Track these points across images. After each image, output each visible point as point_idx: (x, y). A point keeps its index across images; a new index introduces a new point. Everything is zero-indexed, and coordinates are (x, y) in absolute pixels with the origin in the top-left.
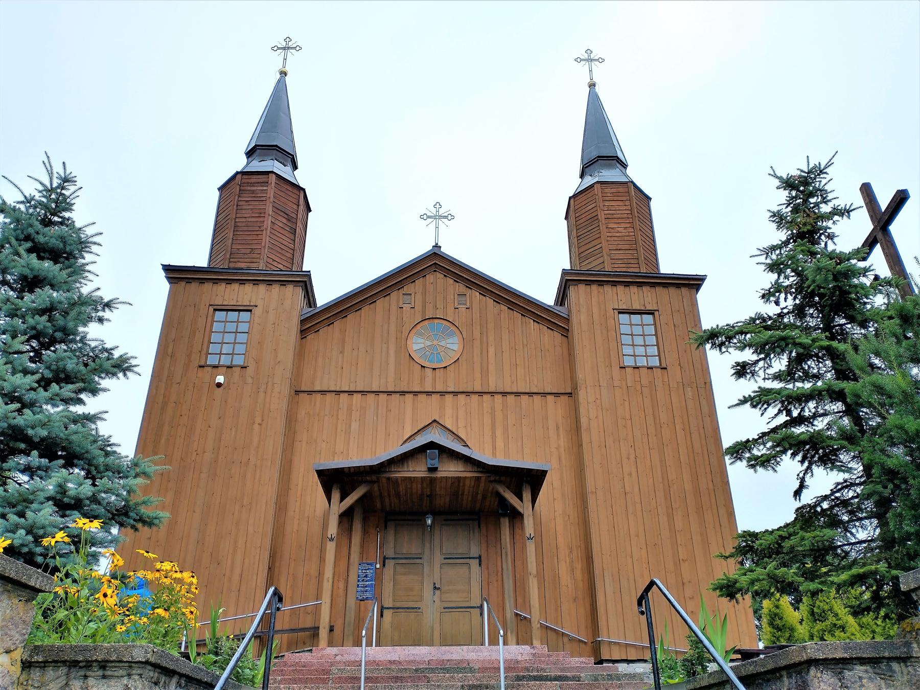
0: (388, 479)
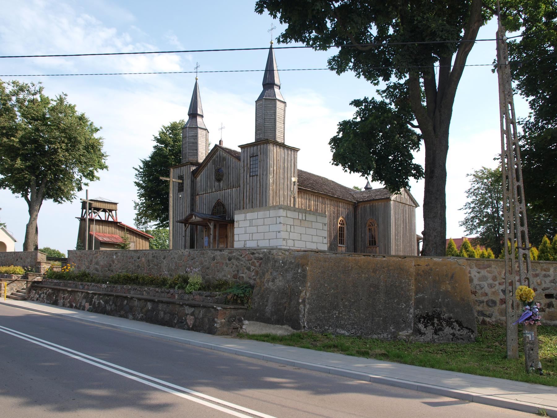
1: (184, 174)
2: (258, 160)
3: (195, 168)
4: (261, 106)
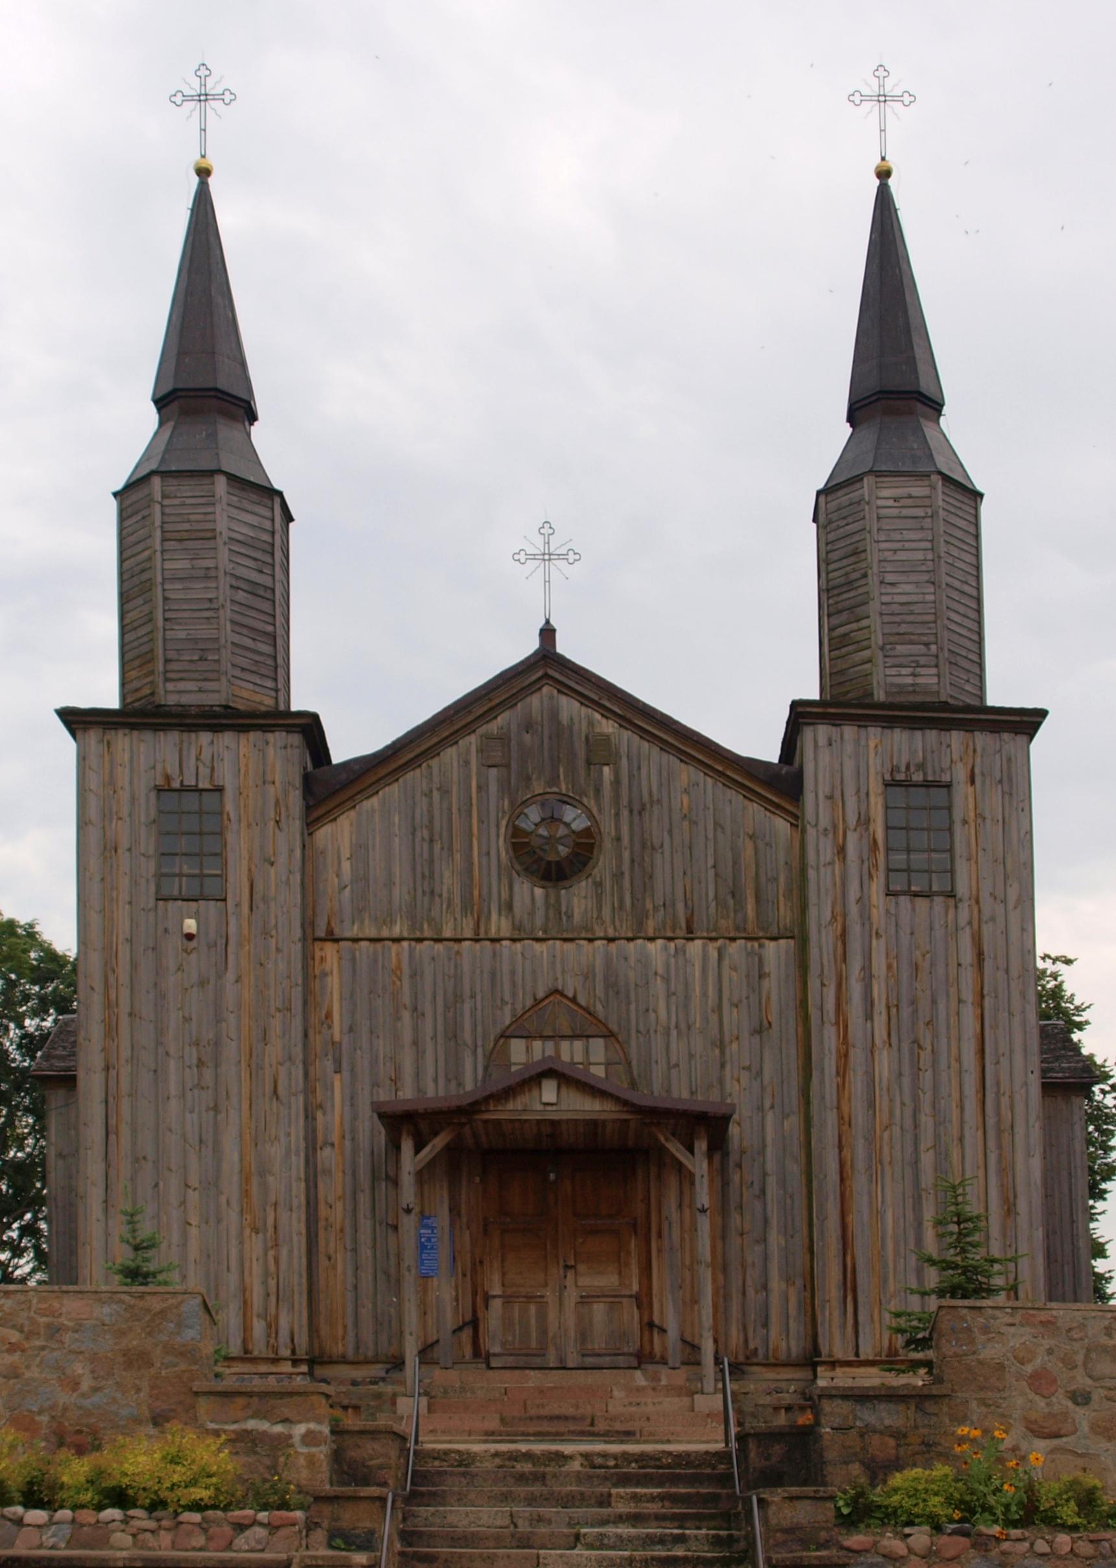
0: (486, 1121)
4: (919, 512)
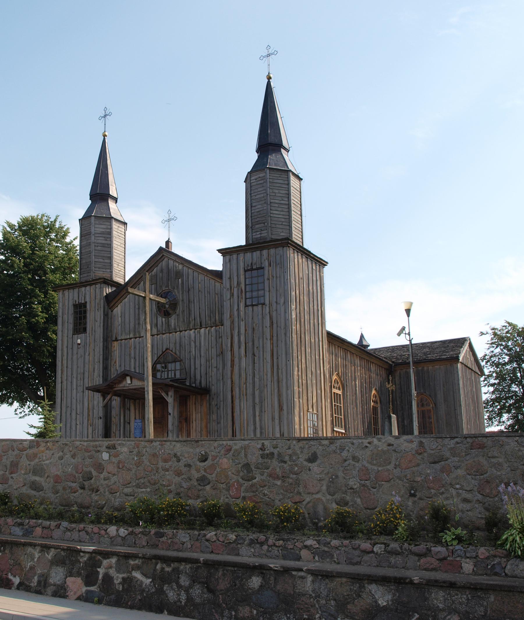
1: (88, 300)
2: (264, 275)
3: (110, 291)
4: (262, 182)
